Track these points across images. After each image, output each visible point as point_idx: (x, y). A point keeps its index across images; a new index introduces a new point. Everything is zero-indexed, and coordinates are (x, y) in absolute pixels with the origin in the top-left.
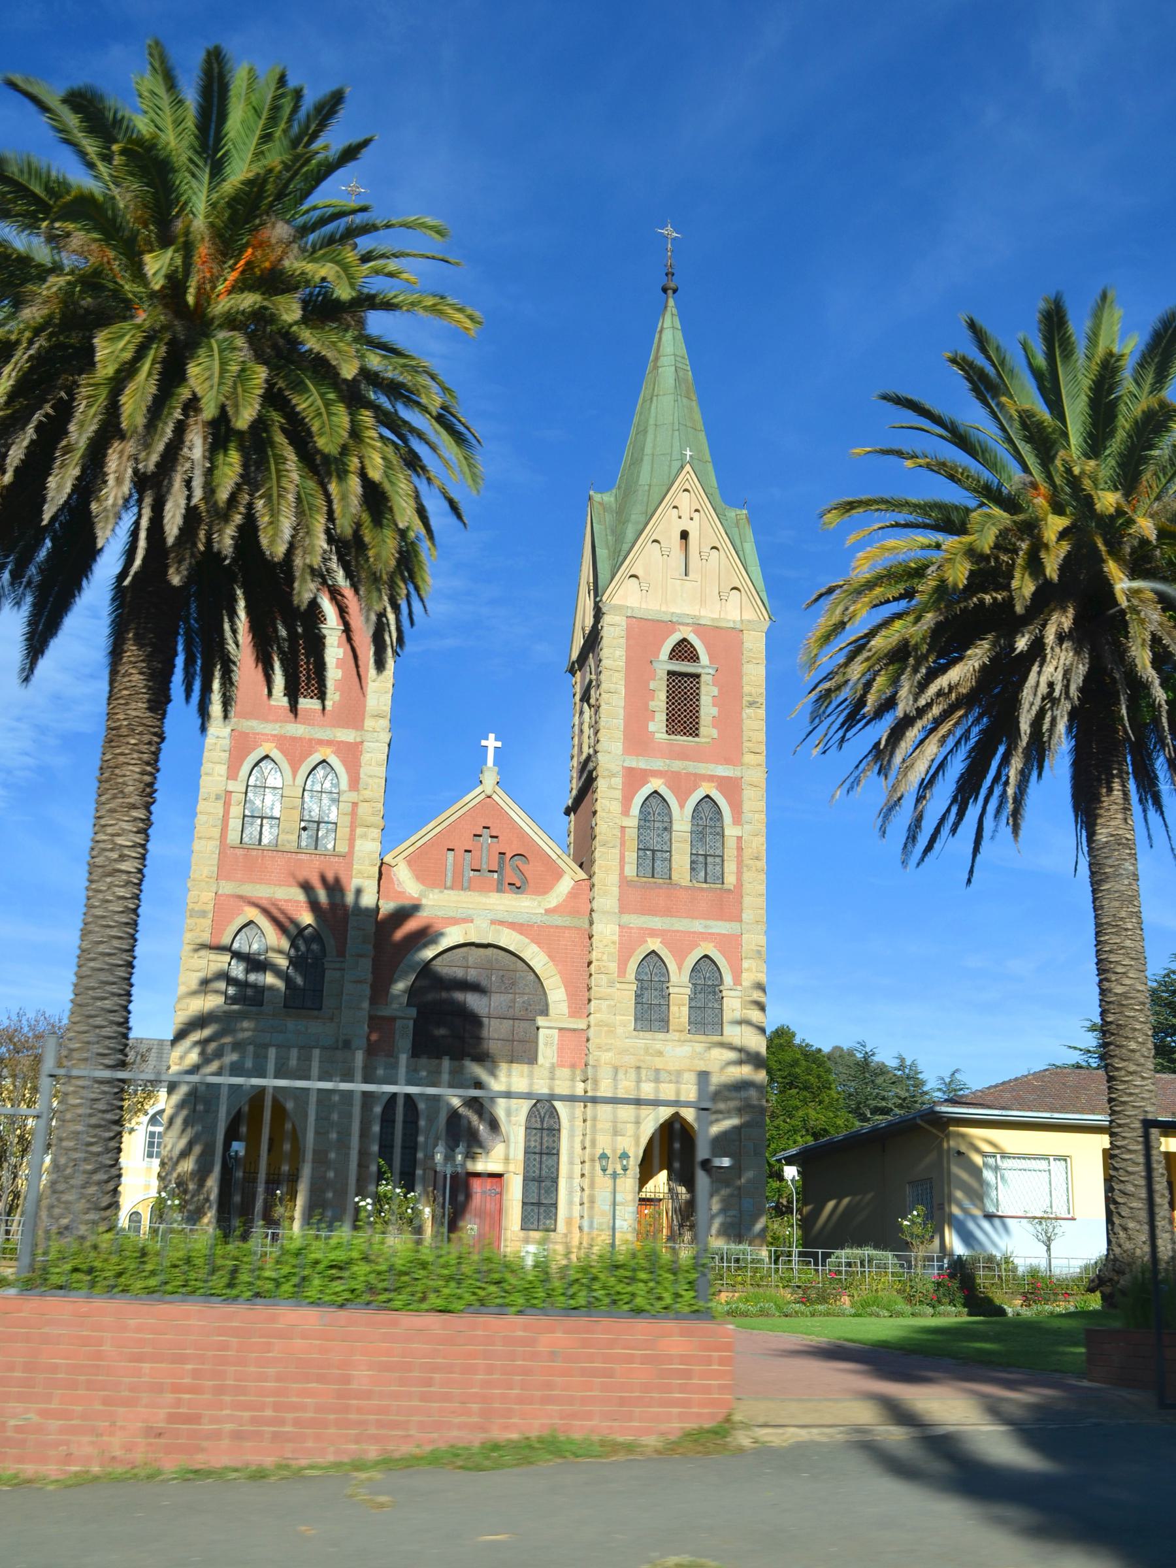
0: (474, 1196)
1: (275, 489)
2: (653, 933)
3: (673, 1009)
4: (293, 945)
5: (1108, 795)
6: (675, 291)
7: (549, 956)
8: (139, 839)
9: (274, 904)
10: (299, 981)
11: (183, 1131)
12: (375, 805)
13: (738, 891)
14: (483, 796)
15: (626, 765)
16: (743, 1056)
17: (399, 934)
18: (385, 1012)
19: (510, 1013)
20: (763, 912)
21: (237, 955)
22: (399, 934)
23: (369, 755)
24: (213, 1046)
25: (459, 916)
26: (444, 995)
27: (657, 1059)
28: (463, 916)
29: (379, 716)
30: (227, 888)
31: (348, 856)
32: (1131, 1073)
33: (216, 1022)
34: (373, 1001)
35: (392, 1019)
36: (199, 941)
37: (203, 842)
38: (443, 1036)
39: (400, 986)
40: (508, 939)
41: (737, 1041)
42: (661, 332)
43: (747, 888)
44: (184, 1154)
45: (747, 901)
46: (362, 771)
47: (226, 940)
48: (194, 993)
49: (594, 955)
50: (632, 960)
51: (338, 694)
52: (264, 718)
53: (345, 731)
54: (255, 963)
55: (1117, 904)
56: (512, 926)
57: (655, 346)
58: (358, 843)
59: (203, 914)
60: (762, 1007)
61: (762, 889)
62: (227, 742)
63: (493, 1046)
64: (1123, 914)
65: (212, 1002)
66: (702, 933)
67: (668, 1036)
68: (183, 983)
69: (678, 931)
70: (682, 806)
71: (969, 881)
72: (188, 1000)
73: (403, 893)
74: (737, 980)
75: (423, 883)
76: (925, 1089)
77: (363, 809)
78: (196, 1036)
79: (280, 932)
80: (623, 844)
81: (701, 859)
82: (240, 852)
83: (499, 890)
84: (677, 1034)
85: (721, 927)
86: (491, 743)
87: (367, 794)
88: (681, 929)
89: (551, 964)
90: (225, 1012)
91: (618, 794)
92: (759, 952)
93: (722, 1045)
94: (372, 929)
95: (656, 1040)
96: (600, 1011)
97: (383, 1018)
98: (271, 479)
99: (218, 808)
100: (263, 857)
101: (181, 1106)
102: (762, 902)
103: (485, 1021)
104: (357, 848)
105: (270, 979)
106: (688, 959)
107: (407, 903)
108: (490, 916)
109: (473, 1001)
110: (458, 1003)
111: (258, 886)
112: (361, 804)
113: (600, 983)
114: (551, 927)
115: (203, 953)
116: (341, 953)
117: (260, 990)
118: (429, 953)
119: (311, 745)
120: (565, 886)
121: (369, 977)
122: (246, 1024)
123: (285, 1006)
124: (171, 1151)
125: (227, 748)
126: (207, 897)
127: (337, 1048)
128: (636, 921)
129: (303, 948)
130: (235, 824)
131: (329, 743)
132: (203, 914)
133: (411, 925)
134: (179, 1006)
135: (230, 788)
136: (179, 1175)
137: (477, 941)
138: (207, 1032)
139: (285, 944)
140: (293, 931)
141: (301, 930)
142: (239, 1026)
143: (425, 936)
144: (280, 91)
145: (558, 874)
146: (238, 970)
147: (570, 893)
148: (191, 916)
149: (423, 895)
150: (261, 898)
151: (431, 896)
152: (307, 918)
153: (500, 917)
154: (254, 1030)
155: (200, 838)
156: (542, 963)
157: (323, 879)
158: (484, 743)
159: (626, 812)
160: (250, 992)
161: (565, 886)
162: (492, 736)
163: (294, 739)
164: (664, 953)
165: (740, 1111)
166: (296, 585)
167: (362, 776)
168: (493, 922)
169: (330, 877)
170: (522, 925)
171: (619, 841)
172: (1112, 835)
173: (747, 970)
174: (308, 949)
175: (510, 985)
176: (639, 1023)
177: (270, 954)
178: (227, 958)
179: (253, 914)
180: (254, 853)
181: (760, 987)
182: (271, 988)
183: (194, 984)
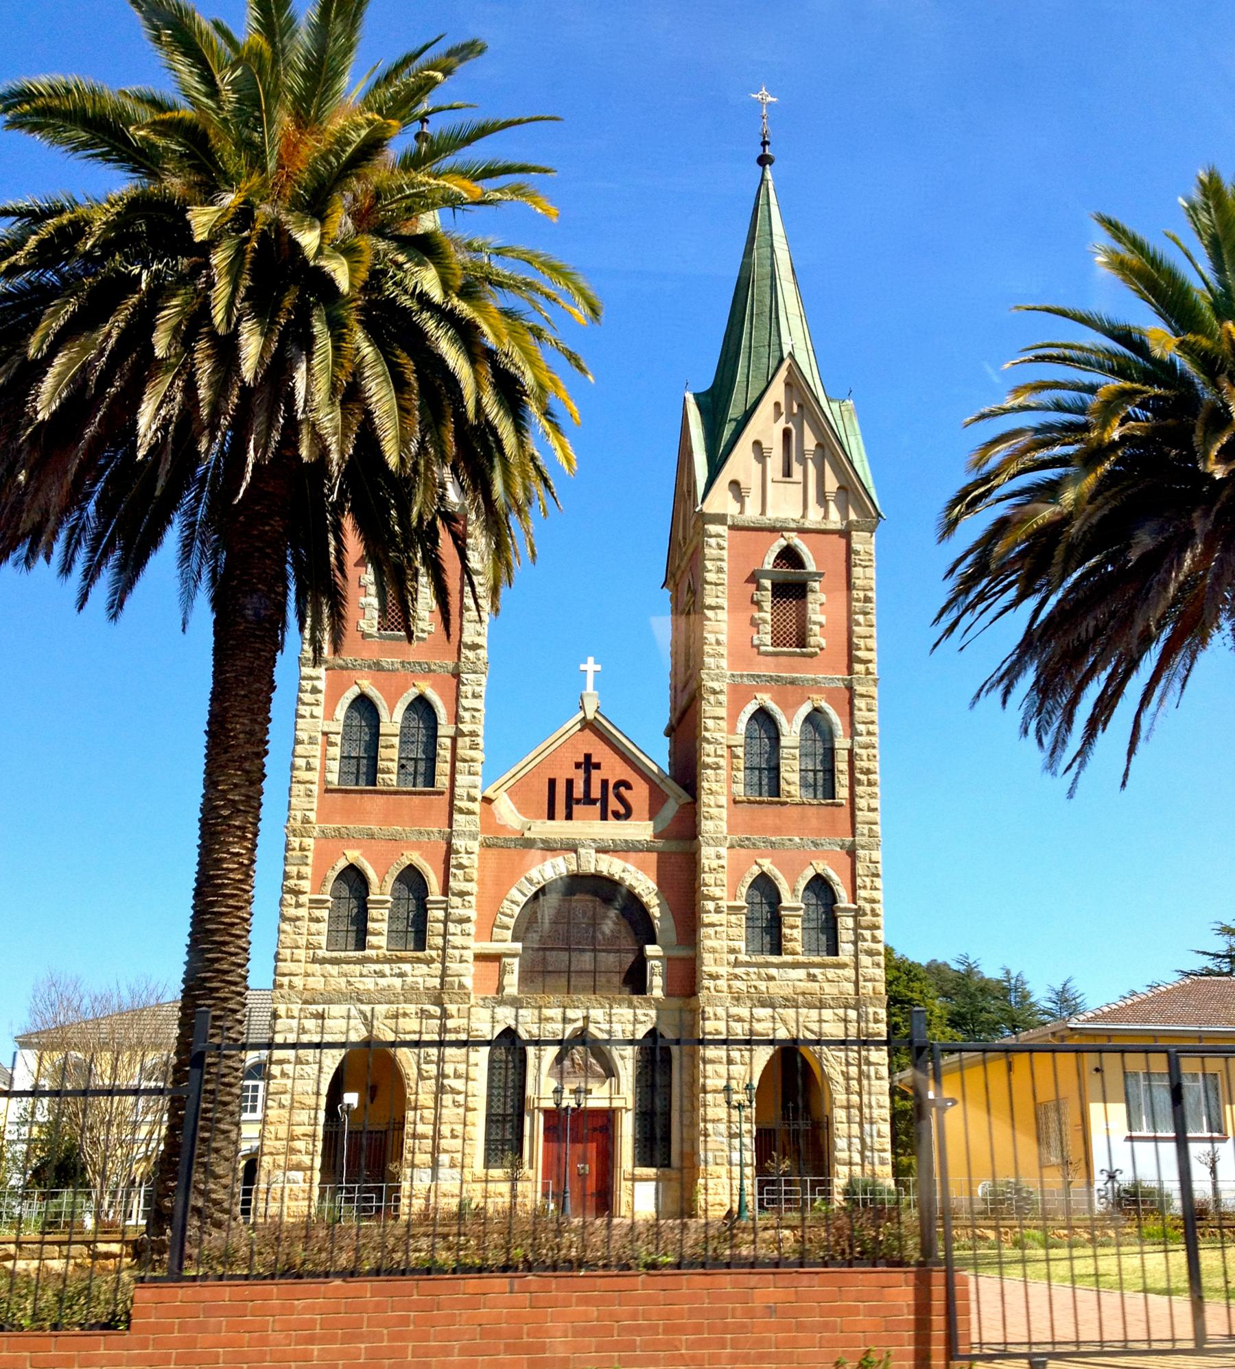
8: (284, 967)
70: (790, 721)
71: (1124, 784)
75: (524, 814)
76: (1032, 1000)
83: (604, 817)
86: (591, 666)
158: (583, 667)
162: (591, 660)
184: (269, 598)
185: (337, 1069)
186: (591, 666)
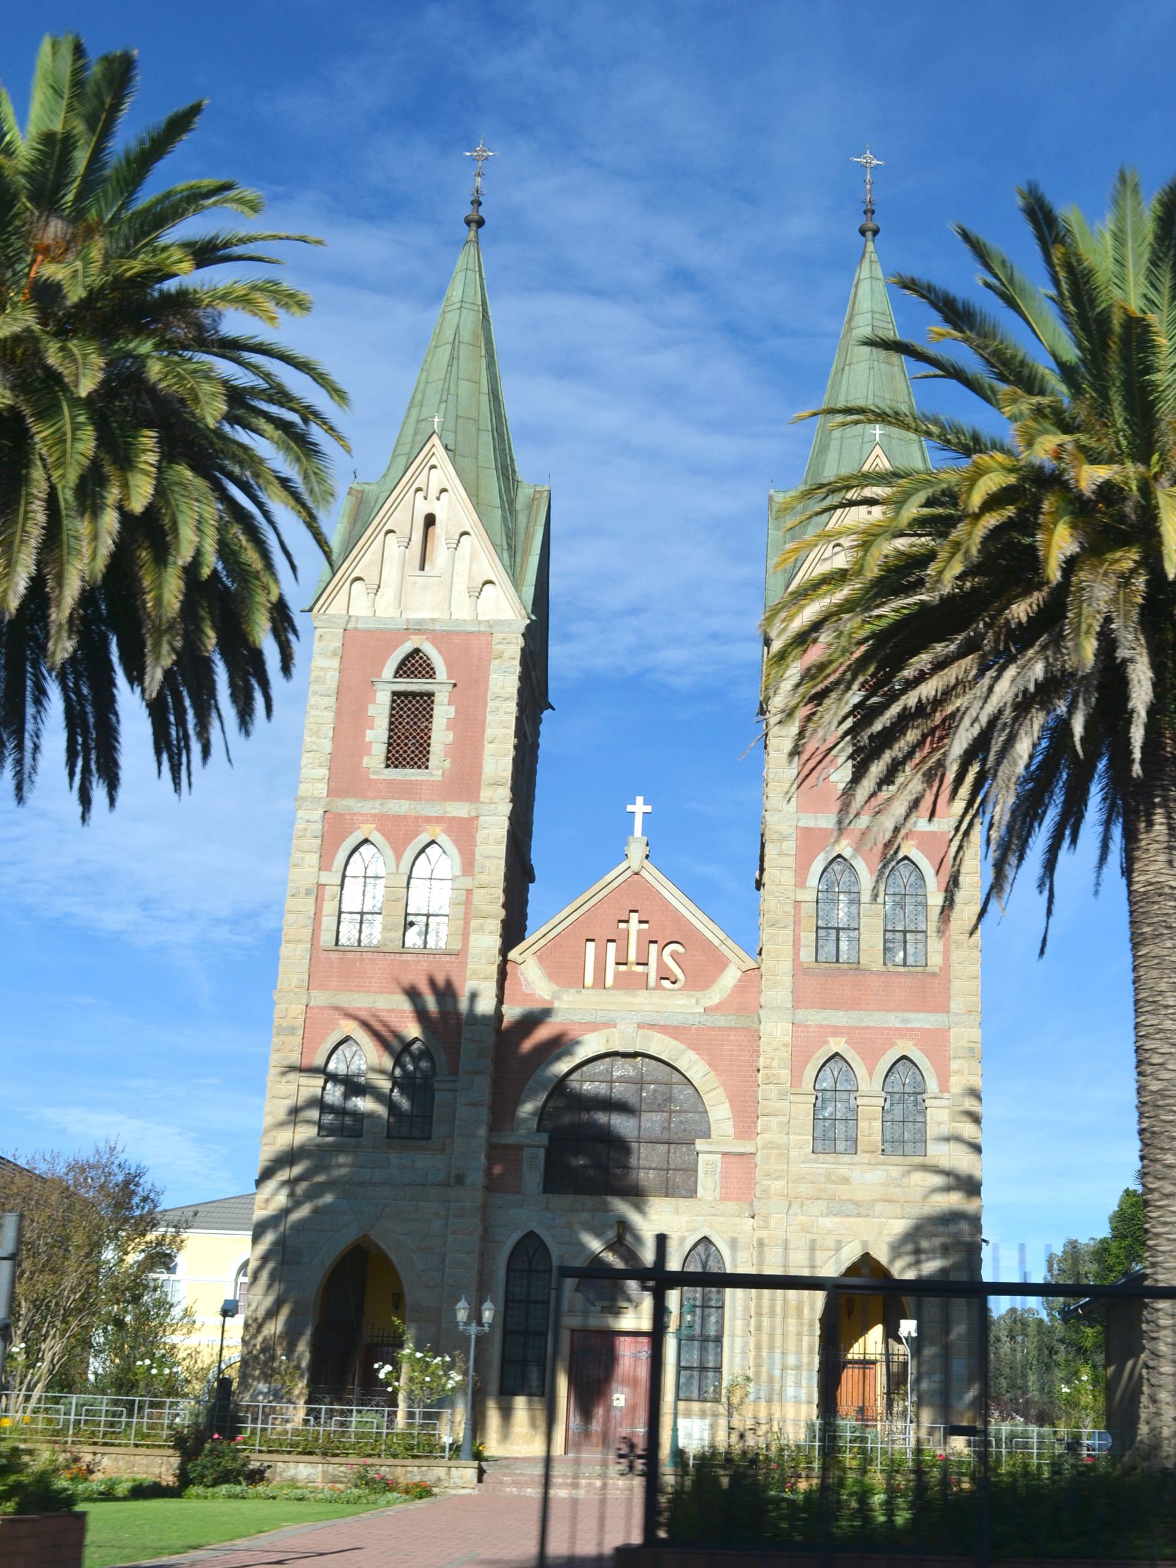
0: (621, 1362)
1: (19, 534)
2: (836, 1031)
3: (862, 1124)
4: (398, 1062)
5: (1147, 832)
6: (876, 232)
7: (710, 1065)
9: (374, 1016)
10: (405, 1104)
11: (269, 1287)
12: (492, 891)
13: (944, 975)
14: (629, 873)
15: (801, 824)
16: (952, 1181)
17: (527, 1045)
18: (510, 1139)
19: (665, 1136)
20: (977, 999)
21: (332, 1077)
22: (527, 1045)
23: (486, 831)
24: (301, 1188)
25: (599, 1020)
26: (585, 1117)
27: (841, 1187)
28: (604, 1020)
29: (496, 784)
30: (320, 998)
31: (460, 955)
32: (1167, 1196)
33: (308, 1157)
34: (493, 1127)
35: (520, 1148)
36: (287, 1063)
37: (291, 946)
38: (582, 1166)
39: (528, 1108)
40: (659, 1045)
41: (945, 1163)
42: (857, 285)
43: (956, 970)
44: (272, 1314)
45: (956, 985)
46: (477, 850)
47: (319, 1061)
48: (282, 1124)
49: (762, 1062)
50: (809, 1065)
51: (449, 760)
52: (362, 795)
53: (457, 804)
54: (353, 1086)
55: (1155, 973)
56: (665, 1029)
57: (850, 303)
58: (473, 937)
59: (292, 1031)
60: (976, 1119)
61: (976, 970)
62: (319, 826)
63: (647, 1177)
64: (1163, 986)
65: (305, 1134)
66: (897, 1029)
67: (856, 1158)
68: (270, 1113)
69: (868, 1028)
71: (1042, 952)
72: (274, 1133)
73: (533, 995)
74: (944, 1086)
75: (557, 983)
77: (479, 897)
78: (284, 1175)
79: (380, 1048)
80: (797, 922)
81: (899, 936)
82: (334, 956)
84: (867, 1155)
85: (922, 1021)
87: (483, 878)
88: (872, 1024)
89: (712, 1074)
90: (317, 1145)
91: (790, 861)
92: (971, 1049)
93: (925, 1168)
94: (490, 1040)
95: (842, 1165)
96: (769, 1130)
97: (507, 1147)
98: (17, 523)
99: (309, 905)
100: (362, 959)
101: (265, 1259)
102: (975, 986)
103: (634, 1145)
104: (471, 944)
105: (364, 1104)
106: (881, 1061)
107: (536, 1006)
108: (638, 1018)
109: (621, 1124)
110: (602, 1125)
111: (356, 995)
112: (475, 891)
113: (768, 1096)
114: (712, 1028)
115: (292, 1076)
116: (454, 1071)
117: (358, 1116)
118: (562, 1067)
119: (415, 824)
120: (730, 978)
121: (486, 1097)
122: (342, 1159)
123: (389, 1136)
124: (256, 1310)
125: (319, 833)
126: (297, 1009)
127: (449, 1185)
128: (814, 1017)
129: (410, 1067)
130: (329, 922)
131: (439, 820)
132: (292, 1031)
133: (542, 1034)
134: (265, 1140)
135: (323, 881)
136: (265, 1339)
137: (621, 1050)
138: (297, 1170)
139: (388, 1062)
140: (397, 1046)
141: (407, 1046)
142: (334, 1161)
143: (559, 1046)
144: (80, 63)
145: (721, 964)
146: (334, 1094)
147: (736, 986)
148: (278, 1034)
149: (556, 996)
150: (360, 1009)
151: (565, 997)
152: (412, 1030)
153: (648, 1019)
154: (352, 1166)
155: (288, 942)
156: (701, 1073)
157: (432, 983)
158: (630, 808)
159: (801, 883)
160: (348, 1121)
161: (730, 978)
163: (397, 818)
164: (850, 1055)
165: (945, 1250)
166: (50, 645)
167: (477, 857)
168: (640, 1026)
169: (440, 980)
170: (677, 1027)
171: (792, 919)
172: (1151, 884)
173: (957, 1073)
174: (416, 1067)
175: (664, 1103)
176: (819, 1143)
177: (371, 1075)
178: (320, 1081)
179: (350, 1027)
180: (351, 955)
181: (975, 1094)
182: (371, 1115)
183: (281, 1114)
184: (17, 1194)
185: (448, 632)
186: (639, 807)
